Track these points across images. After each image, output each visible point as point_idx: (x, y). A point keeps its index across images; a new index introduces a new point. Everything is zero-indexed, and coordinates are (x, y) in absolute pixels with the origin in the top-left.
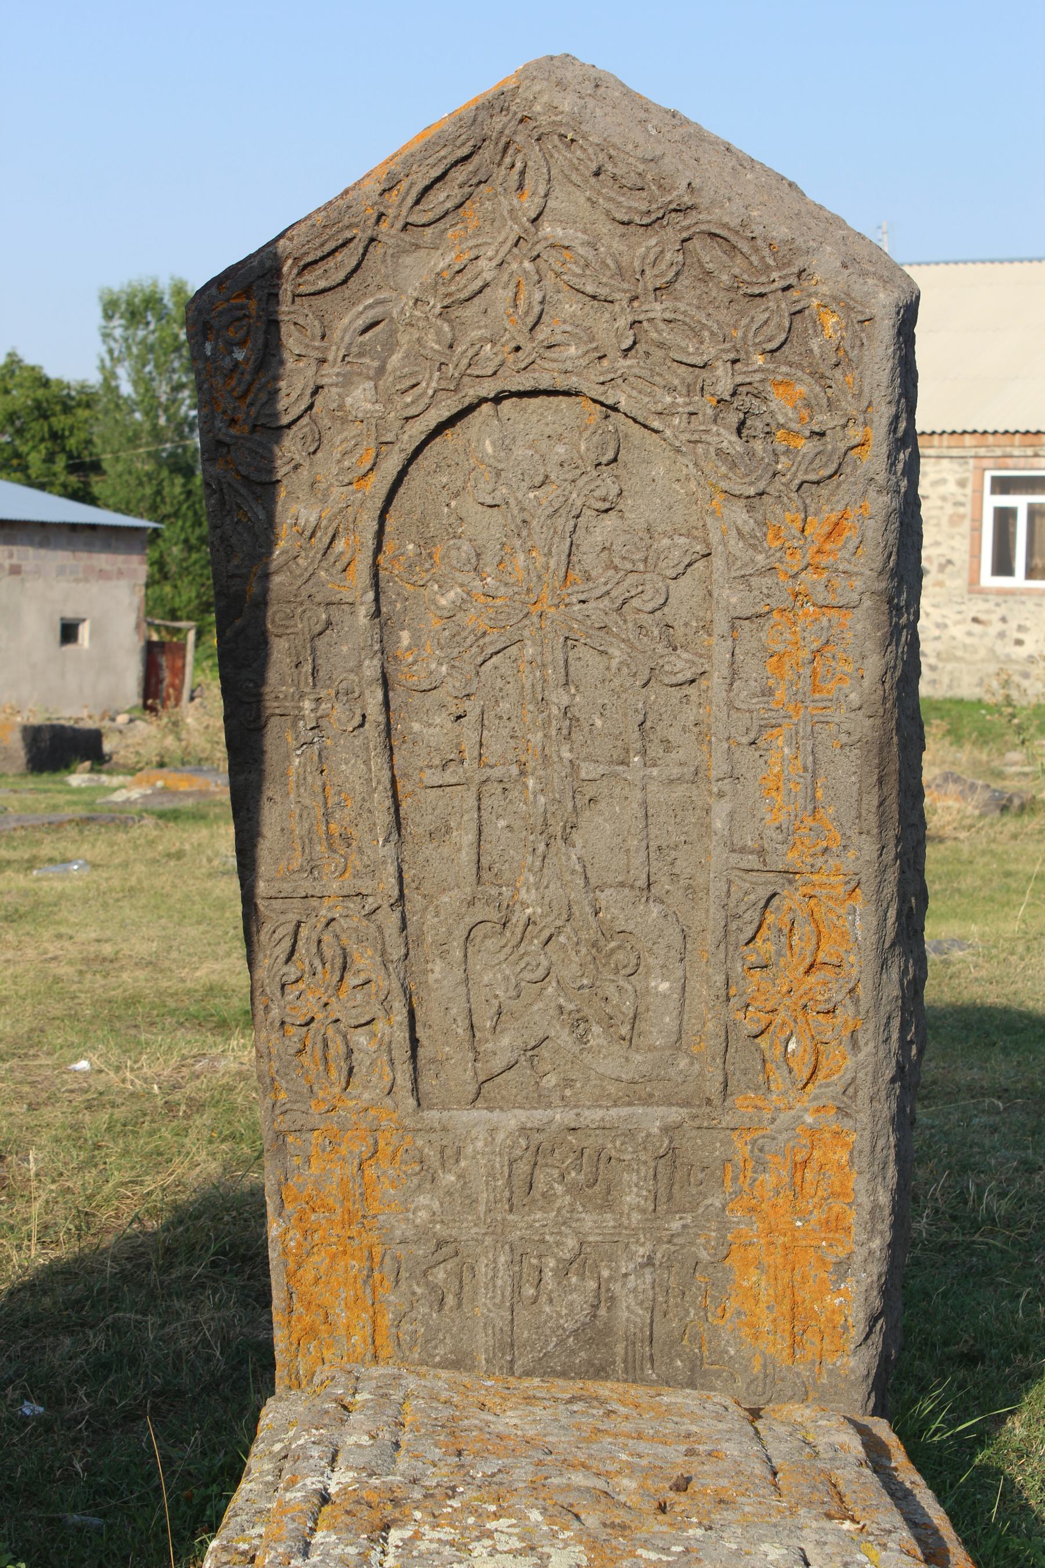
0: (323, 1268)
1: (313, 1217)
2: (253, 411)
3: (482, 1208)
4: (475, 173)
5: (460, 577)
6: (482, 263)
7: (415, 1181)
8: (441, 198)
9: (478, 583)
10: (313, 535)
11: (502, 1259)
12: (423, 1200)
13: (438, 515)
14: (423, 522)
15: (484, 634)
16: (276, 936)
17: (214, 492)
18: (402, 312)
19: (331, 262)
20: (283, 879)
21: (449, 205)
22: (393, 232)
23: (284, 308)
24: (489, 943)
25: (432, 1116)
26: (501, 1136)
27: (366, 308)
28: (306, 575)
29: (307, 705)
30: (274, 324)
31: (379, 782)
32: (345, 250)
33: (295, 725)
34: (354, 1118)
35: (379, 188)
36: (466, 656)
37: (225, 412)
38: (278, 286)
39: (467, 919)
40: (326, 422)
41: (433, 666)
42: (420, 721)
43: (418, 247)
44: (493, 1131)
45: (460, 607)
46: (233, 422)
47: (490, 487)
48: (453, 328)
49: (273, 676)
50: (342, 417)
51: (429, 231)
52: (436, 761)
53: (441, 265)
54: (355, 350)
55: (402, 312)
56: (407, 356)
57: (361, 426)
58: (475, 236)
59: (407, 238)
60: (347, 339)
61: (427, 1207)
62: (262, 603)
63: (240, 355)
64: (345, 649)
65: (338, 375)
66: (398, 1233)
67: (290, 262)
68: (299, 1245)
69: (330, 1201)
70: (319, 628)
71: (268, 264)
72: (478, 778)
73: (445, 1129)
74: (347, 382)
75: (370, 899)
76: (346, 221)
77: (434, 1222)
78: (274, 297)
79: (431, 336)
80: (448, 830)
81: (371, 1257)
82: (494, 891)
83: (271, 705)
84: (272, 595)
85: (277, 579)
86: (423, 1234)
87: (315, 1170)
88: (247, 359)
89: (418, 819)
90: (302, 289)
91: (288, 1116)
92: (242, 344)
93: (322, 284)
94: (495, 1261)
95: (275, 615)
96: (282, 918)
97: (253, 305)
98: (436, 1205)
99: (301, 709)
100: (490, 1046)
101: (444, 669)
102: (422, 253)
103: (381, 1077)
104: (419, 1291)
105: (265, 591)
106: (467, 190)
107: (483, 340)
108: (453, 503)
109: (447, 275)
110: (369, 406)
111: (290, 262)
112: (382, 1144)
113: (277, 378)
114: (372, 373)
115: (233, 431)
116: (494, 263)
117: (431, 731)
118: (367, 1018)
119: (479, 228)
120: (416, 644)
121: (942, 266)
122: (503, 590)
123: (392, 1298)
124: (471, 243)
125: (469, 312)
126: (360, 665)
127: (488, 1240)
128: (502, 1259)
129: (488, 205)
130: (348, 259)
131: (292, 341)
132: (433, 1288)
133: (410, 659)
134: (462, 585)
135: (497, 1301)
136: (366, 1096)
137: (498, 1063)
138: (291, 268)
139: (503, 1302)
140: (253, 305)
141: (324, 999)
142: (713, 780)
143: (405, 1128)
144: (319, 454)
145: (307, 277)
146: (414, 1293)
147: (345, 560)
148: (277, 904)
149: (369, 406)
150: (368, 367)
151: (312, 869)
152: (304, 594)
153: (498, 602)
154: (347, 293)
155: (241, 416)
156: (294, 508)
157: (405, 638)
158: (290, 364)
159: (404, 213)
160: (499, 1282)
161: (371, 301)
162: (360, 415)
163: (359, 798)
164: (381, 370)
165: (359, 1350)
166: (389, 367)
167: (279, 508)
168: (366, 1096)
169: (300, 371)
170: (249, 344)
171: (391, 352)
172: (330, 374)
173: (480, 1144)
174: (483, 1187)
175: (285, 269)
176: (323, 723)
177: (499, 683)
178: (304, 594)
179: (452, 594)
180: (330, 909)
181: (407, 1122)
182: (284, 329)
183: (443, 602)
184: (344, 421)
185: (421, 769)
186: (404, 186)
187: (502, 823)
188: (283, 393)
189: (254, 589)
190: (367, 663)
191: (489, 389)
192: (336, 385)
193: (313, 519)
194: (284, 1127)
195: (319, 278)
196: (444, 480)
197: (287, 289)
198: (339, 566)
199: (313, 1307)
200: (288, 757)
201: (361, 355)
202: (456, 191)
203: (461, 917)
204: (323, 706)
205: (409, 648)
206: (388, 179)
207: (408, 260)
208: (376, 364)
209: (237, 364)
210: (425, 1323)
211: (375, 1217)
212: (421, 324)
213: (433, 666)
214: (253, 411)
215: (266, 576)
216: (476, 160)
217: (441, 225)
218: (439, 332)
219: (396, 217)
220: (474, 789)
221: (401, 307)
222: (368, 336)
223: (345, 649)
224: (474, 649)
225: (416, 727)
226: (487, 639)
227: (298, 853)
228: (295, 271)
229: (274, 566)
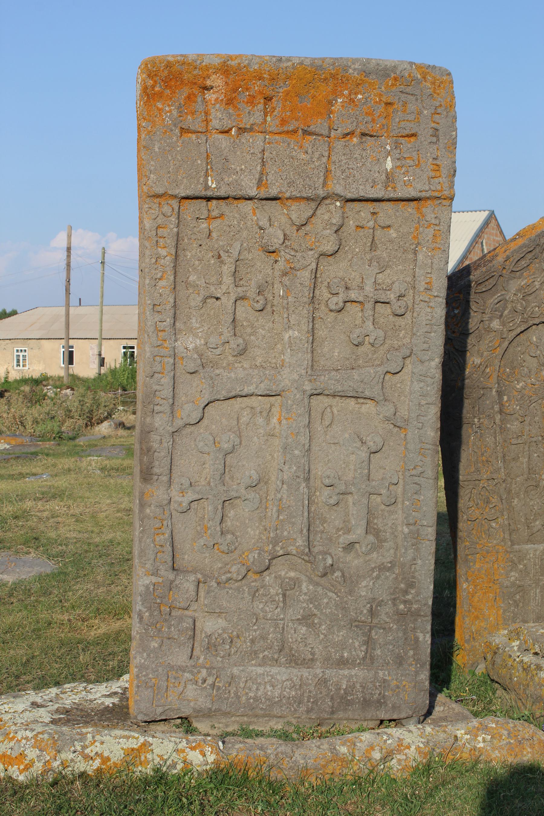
0: (481, 597)
1: (478, 581)
2: (460, 329)
3: (531, 575)
4: (534, 256)
5: (524, 379)
6: (536, 283)
7: (510, 568)
8: (523, 263)
9: (529, 381)
10: (479, 367)
11: (538, 591)
12: (513, 574)
13: (517, 360)
14: (512, 362)
15: (531, 397)
16: (465, 493)
17: (447, 354)
18: (510, 298)
19: (487, 283)
20: (467, 475)
21: (525, 265)
22: (508, 273)
23: (472, 297)
24: (532, 492)
25: (516, 547)
26: (538, 552)
27: (498, 297)
28: (477, 380)
29: (476, 420)
30: (468, 302)
31: (499, 443)
32: (492, 279)
33: (472, 427)
34: (491, 549)
35: (503, 260)
36: (525, 403)
37: (451, 329)
38: (470, 290)
39: (525, 485)
40: (483, 332)
41: (515, 407)
42: (510, 424)
43: (515, 278)
44: (536, 551)
45: (523, 388)
46: (454, 332)
47: (534, 351)
48: (526, 303)
49: (465, 411)
50: (489, 330)
51: (518, 273)
52: (515, 436)
53: (522, 284)
54: (494, 309)
55: (510, 298)
56: (510, 311)
57: (494, 333)
58: (533, 275)
59: (512, 276)
60: (492, 306)
61: (514, 576)
62: (462, 388)
63: (456, 312)
64: (488, 402)
65: (488, 317)
66: (505, 584)
67: (474, 283)
68: (473, 590)
69: (483, 576)
70: (480, 396)
71: (467, 283)
72: (529, 441)
73: (520, 551)
74: (491, 319)
75: (496, 480)
76: (492, 270)
77: (516, 580)
78: (469, 294)
79: (519, 305)
80: (519, 458)
81: (496, 593)
82: (534, 476)
83: (465, 420)
84: (466, 386)
85: (467, 381)
86: (513, 584)
87: (477, 566)
88: (459, 313)
89: (509, 455)
90: (477, 291)
91: (470, 550)
92: (457, 308)
93: (484, 289)
94: (536, 592)
95: (466, 391)
96: (468, 487)
97: (461, 296)
98: (517, 575)
99: (474, 421)
100: (532, 524)
101: (518, 407)
102: (516, 280)
103: (500, 536)
104: (511, 602)
105: (463, 385)
106: (531, 260)
107: (536, 306)
108: (522, 356)
109: (524, 287)
110: (498, 327)
111: (474, 283)
112: (499, 557)
113: (468, 318)
114: (498, 316)
115: (453, 335)
116: (540, 283)
117: (513, 427)
118: (495, 517)
119: (534, 272)
120: (509, 400)
121: (470, 213)
122: (537, 383)
123: (502, 605)
124: (532, 277)
125: (530, 298)
126: (493, 407)
127: (534, 585)
128: (538, 591)
129: (537, 265)
130: (492, 282)
131: (473, 306)
132: (515, 601)
133: (507, 405)
134: (524, 381)
135: (536, 604)
136: (495, 542)
137: (535, 529)
138: (474, 285)
139: (538, 604)
140: (461, 296)
141: (482, 512)
142: (137, 432)
143: (507, 552)
144: (481, 342)
145: (479, 287)
146: (509, 603)
147: (489, 375)
148: (466, 483)
149: (498, 327)
150: (497, 315)
151: (478, 470)
152: (476, 385)
153: (536, 386)
154: (491, 292)
155: (456, 330)
156: (472, 359)
157: (505, 398)
158: (472, 314)
159: (511, 267)
160: (537, 598)
161: (499, 295)
162: (495, 330)
163: (492, 449)
164: (501, 316)
165: (493, 622)
166: (504, 315)
167: (467, 359)
168: (495, 542)
169: (476, 316)
170: (460, 308)
171: (505, 310)
172: (486, 317)
173: (531, 555)
174: (532, 569)
175: (472, 285)
176: (481, 426)
177: (535, 411)
178: (476, 385)
179: (521, 384)
180: (483, 484)
181: (508, 549)
182: (471, 304)
183: (518, 387)
184: (488, 331)
185: (510, 439)
186: (512, 259)
187: (536, 455)
188: (470, 323)
189: (460, 384)
190: (495, 406)
191: (537, 321)
192: (488, 320)
193: (479, 362)
194: (468, 553)
195: (483, 288)
196: (519, 349)
197: (473, 291)
198: (487, 377)
199: (478, 610)
200: (469, 437)
201: (495, 311)
202: (528, 261)
203: (523, 484)
204: (481, 420)
205: (507, 401)
206: (506, 258)
207: (511, 282)
208: (500, 314)
209: (455, 315)
210: (513, 612)
211: (498, 580)
212: (516, 302)
213: (515, 407)
214: (460, 329)
215: (463, 380)
216: (534, 252)
217: (522, 271)
218: (522, 304)
219: (509, 269)
220: (528, 444)
221: (510, 296)
222: (498, 305)
223: (488, 402)
224: (528, 401)
225: (508, 426)
226: (532, 398)
227: (473, 467)
228: (475, 286)
229: (466, 376)
